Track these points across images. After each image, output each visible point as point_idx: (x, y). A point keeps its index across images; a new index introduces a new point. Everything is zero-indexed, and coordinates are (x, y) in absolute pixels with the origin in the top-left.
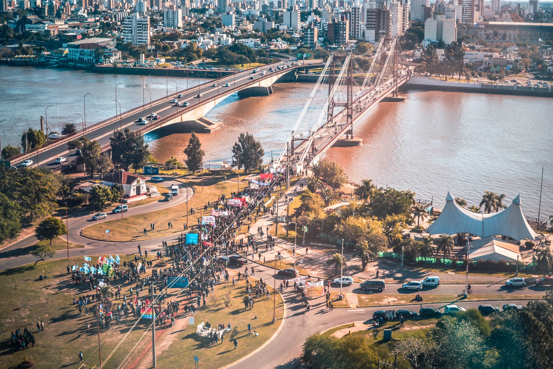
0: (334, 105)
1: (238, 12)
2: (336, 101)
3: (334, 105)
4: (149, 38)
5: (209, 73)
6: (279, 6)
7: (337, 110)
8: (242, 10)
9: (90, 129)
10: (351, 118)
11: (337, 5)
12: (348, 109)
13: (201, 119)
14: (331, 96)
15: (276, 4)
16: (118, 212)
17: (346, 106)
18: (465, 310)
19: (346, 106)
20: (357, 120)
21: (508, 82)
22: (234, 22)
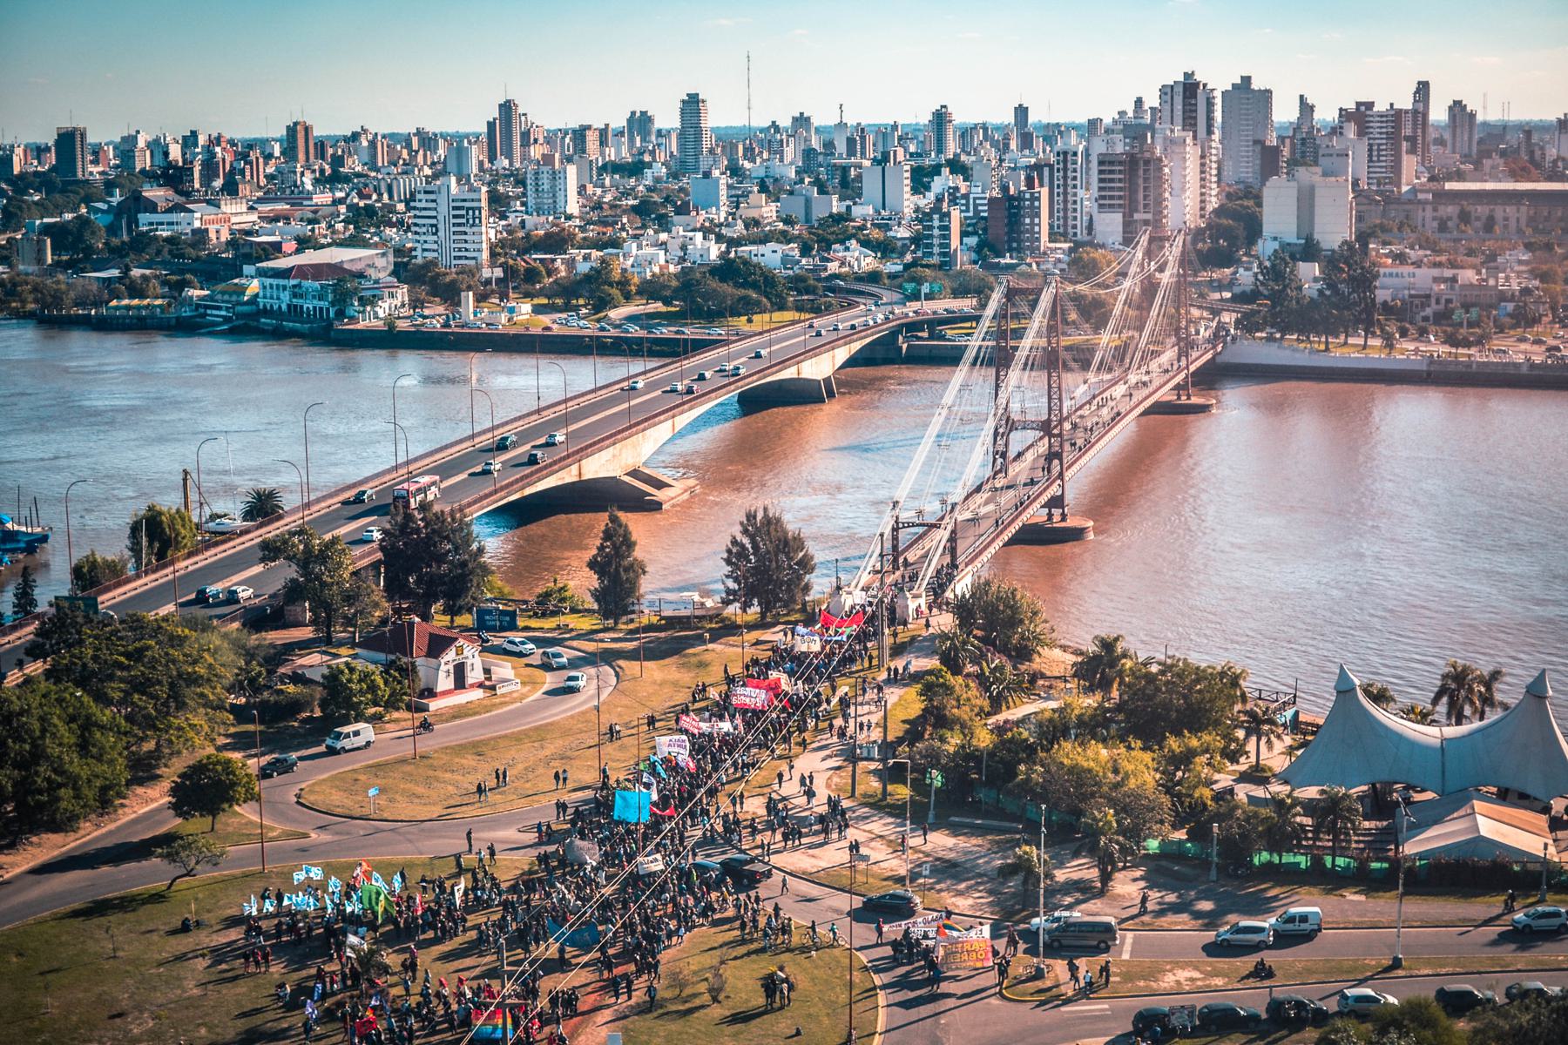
0: (1011, 425)
2: (1015, 416)
3: (1011, 425)
4: (485, 246)
7: (1018, 440)
9: (323, 505)
13: (634, 473)
14: (1002, 401)
17: (1046, 427)
19: (1046, 427)
22: (723, 199)
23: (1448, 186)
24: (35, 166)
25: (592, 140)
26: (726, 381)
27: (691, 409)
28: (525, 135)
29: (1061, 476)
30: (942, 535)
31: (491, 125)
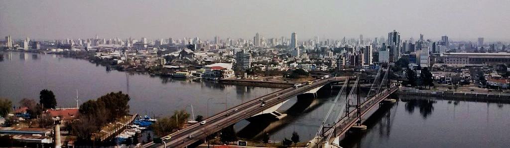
0: (350, 106)
1: (302, 47)
2: (350, 104)
3: (350, 106)
4: (250, 63)
5: (275, 87)
6: (326, 44)
7: (351, 109)
8: (305, 46)
9: (244, 111)
10: (360, 114)
11: (359, 43)
12: (358, 108)
13: (274, 112)
14: (348, 99)
15: (324, 43)
16: (32, 127)
17: (357, 107)
18: (10, 114)
19: (357, 107)
20: (364, 115)
21: (461, 90)
22: (299, 54)
23: (451, 53)
24: (165, 43)
25: (274, 40)
26: (484, 91)
27: (8, 130)
28: (261, 40)
29: (360, 117)
30: (333, 130)
31: (255, 37)
